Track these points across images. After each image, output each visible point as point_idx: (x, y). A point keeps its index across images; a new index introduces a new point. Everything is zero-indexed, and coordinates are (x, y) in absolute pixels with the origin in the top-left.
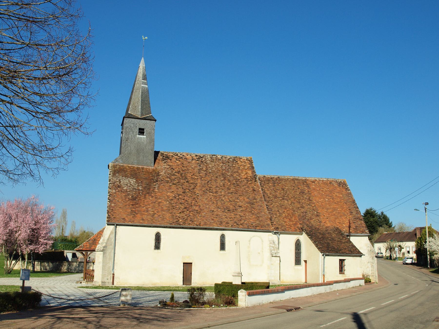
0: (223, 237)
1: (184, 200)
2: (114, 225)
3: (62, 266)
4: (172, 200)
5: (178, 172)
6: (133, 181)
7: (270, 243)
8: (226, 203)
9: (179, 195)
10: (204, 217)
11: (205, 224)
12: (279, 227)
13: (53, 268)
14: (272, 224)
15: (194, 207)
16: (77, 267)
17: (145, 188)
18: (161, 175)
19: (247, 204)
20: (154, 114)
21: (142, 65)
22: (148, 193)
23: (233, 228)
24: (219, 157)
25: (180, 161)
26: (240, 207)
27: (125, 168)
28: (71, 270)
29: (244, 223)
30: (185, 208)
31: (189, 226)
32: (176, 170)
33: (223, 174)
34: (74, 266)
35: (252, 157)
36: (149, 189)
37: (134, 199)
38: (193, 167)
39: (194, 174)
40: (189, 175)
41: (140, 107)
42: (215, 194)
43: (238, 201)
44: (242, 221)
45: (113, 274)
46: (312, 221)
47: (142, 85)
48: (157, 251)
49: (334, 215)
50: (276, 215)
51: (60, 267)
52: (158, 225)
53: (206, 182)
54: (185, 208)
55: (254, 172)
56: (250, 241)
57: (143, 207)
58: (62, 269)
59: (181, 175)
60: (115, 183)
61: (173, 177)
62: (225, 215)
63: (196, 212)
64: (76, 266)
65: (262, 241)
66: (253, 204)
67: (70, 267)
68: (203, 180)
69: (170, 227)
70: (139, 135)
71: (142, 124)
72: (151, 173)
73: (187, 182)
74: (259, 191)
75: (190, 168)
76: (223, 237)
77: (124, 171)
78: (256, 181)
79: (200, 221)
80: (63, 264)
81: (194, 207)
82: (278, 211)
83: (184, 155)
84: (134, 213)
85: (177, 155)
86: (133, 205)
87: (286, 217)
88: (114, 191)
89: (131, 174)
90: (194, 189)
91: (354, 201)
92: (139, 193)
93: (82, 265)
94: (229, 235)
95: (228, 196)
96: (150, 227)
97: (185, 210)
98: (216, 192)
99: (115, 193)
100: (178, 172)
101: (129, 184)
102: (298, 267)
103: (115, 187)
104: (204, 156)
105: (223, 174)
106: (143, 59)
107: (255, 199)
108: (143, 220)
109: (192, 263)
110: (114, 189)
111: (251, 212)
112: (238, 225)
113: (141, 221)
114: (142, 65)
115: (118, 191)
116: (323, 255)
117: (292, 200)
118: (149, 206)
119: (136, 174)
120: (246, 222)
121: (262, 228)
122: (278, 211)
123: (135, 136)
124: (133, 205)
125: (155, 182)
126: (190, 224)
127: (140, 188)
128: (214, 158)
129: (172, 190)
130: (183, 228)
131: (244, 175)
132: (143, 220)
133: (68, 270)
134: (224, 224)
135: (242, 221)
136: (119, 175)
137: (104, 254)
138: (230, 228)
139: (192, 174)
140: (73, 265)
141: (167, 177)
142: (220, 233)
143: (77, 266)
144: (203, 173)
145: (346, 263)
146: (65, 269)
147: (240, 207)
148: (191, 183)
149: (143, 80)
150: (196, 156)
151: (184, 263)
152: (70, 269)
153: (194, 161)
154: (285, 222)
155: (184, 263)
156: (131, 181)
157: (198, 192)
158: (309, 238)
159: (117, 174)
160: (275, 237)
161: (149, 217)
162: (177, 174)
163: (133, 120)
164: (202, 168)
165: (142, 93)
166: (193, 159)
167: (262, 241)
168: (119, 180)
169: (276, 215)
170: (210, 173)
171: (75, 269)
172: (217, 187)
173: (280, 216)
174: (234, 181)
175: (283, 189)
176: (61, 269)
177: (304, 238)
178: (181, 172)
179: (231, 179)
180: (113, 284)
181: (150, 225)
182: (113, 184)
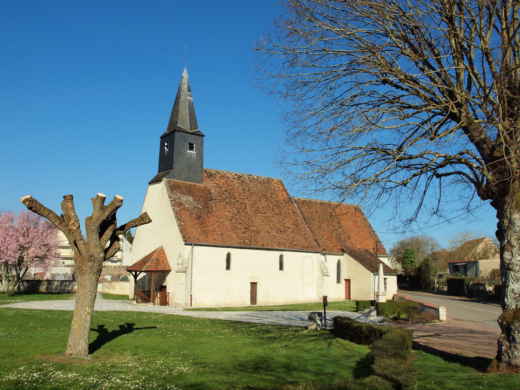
0: (281, 257)
1: (241, 220)
2: (191, 245)
3: (40, 285)
4: (231, 220)
5: (226, 191)
6: (191, 199)
7: (321, 264)
8: (276, 224)
9: (236, 215)
10: (264, 237)
11: (268, 245)
12: (325, 248)
13: (29, 287)
14: (319, 246)
15: (252, 228)
16: (58, 287)
17: (204, 206)
18: (212, 193)
19: (293, 226)
20: (201, 128)
21: (185, 74)
22: (209, 212)
23: (292, 249)
24: (255, 177)
25: (223, 179)
26: (288, 228)
27: (179, 184)
28: (51, 290)
29: (297, 244)
30: (246, 228)
31: (255, 247)
32: (224, 188)
33: (264, 195)
34: (55, 285)
35: (281, 179)
36: (208, 208)
37: (199, 218)
38: (236, 186)
39: (240, 194)
40: (237, 195)
41: (189, 121)
42: (264, 215)
43: (285, 222)
44: (295, 243)
45: (191, 296)
46: (346, 243)
47: (188, 97)
48: (228, 271)
49: (360, 238)
50: (320, 237)
51: (37, 286)
52: (230, 245)
53: (253, 202)
54: (246, 228)
55: (288, 194)
56: (303, 261)
57: (210, 226)
58: (40, 288)
59: (230, 194)
60: (176, 200)
61: (224, 196)
62: (280, 236)
63: (255, 232)
64: (57, 285)
65: (313, 262)
66: (297, 226)
67: (50, 287)
68: (249, 200)
69: (240, 248)
70: (189, 150)
71: (192, 139)
72: (203, 190)
73: (237, 201)
74: (298, 213)
75: (235, 188)
76: (281, 257)
77: (179, 187)
78: (292, 203)
79: (262, 241)
80: (41, 284)
81: (252, 228)
82: (320, 233)
83: (224, 174)
84: (204, 232)
85: (219, 173)
86: (200, 224)
87: (327, 239)
88: (178, 209)
89: (187, 191)
90: (245, 209)
91: (370, 225)
92: (201, 212)
93: (64, 284)
94: (287, 255)
95: (275, 217)
96: (223, 247)
97: (246, 230)
98: (265, 213)
99: (180, 211)
100: (226, 191)
101: (188, 202)
102: (339, 285)
103: (177, 204)
104: (242, 175)
105: (264, 195)
106: (185, 70)
107: (297, 221)
108: (215, 240)
109: (256, 283)
110: (178, 207)
111: (299, 233)
112: (293, 246)
113: (214, 241)
114: (185, 74)
115: (182, 209)
116: (374, 275)
117: (327, 223)
118: (214, 226)
119: (191, 191)
120: (298, 243)
121: (313, 249)
122: (320, 233)
123: (186, 151)
124: (200, 224)
125: (210, 201)
126: (255, 244)
127: (199, 206)
128: (252, 180)
129: (228, 210)
130: (250, 248)
131: (281, 197)
132: (215, 240)
133: (47, 290)
134: (282, 244)
135: (295, 243)
136: (177, 192)
137: (186, 274)
138: (289, 249)
139: (238, 193)
140: (53, 284)
141: (219, 196)
142: (279, 253)
143: (59, 285)
144: (247, 194)
145: (387, 281)
146: (44, 288)
147: (288, 228)
148: (241, 203)
149: (188, 91)
150: (236, 175)
151: (251, 283)
152: (50, 288)
153: (235, 181)
154: (328, 244)
155: (251, 283)
156: (189, 199)
157: (250, 212)
158: (354, 259)
159: (174, 191)
160: (322, 257)
161: (219, 237)
162: (225, 193)
163: (184, 133)
164: (245, 188)
165: (189, 105)
166: (234, 178)
167: (313, 262)
168: (179, 197)
169: (320, 237)
170: (253, 193)
171: (56, 289)
172: (263, 208)
173: (322, 238)
174: (275, 202)
175: (317, 212)
176: (39, 289)
177: (346, 259)
178: (229, 191)
179: (272, 200)
180: (191, 306)
181: (223, 245)
182: (174, 201)
